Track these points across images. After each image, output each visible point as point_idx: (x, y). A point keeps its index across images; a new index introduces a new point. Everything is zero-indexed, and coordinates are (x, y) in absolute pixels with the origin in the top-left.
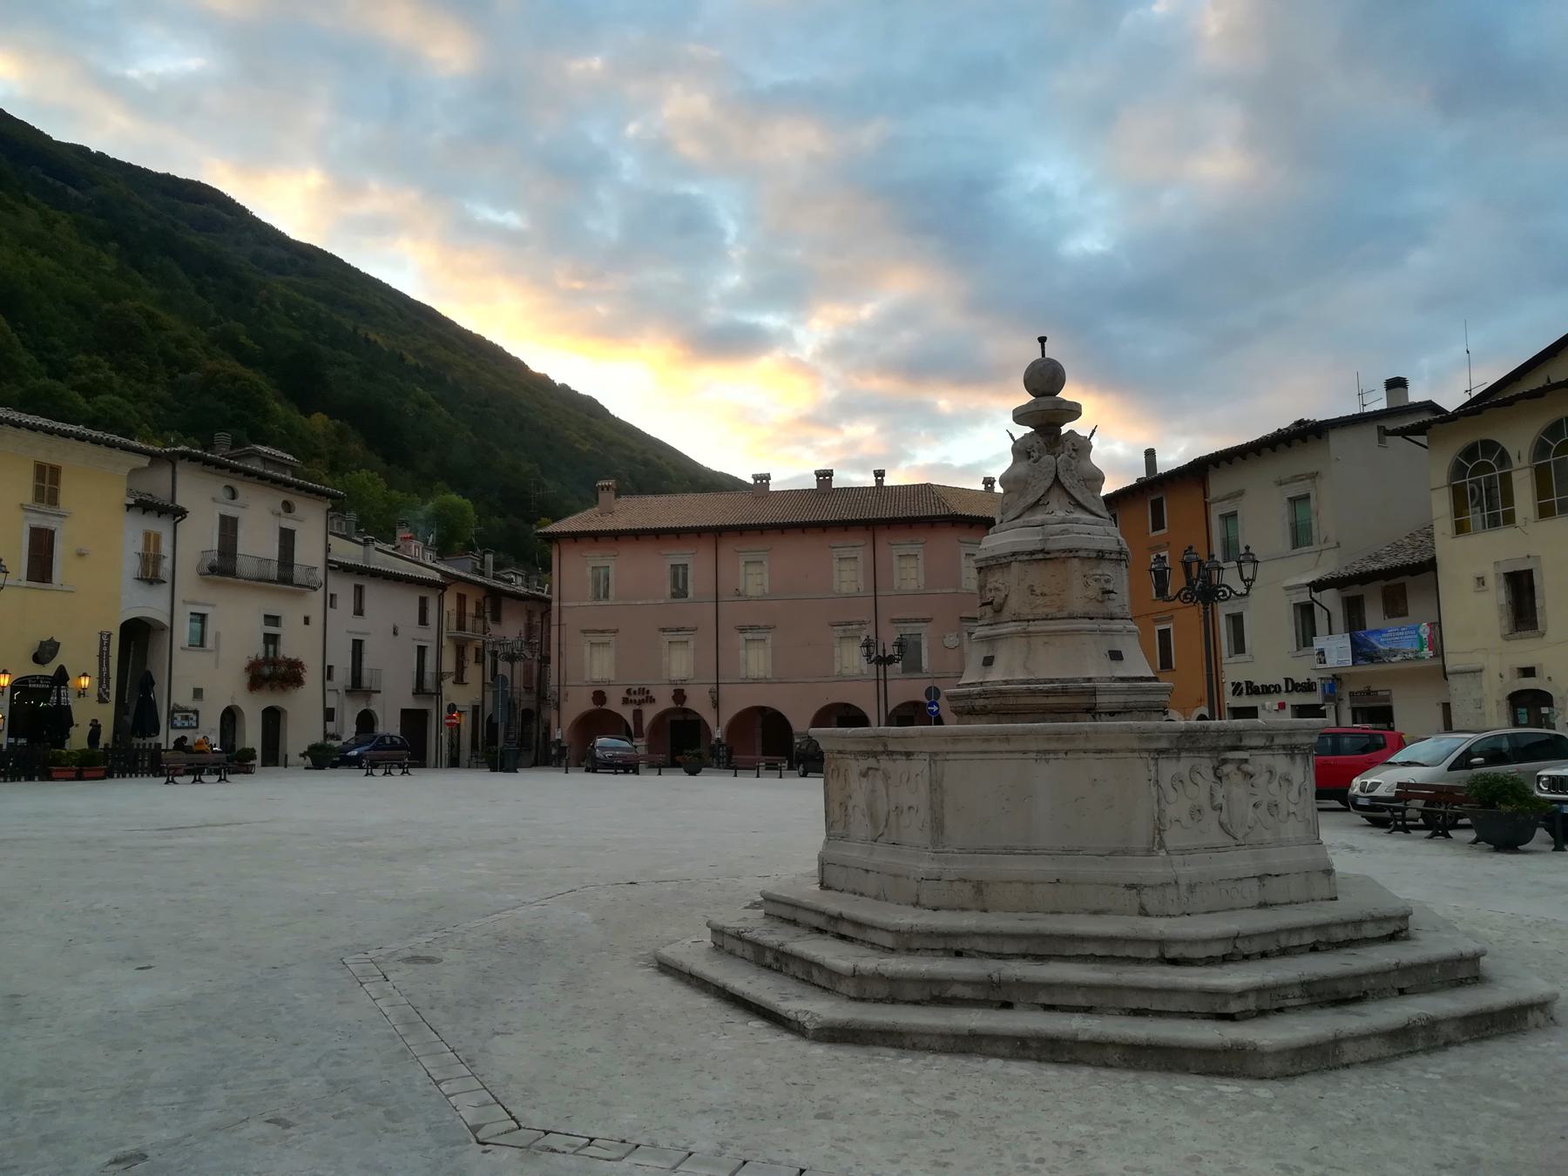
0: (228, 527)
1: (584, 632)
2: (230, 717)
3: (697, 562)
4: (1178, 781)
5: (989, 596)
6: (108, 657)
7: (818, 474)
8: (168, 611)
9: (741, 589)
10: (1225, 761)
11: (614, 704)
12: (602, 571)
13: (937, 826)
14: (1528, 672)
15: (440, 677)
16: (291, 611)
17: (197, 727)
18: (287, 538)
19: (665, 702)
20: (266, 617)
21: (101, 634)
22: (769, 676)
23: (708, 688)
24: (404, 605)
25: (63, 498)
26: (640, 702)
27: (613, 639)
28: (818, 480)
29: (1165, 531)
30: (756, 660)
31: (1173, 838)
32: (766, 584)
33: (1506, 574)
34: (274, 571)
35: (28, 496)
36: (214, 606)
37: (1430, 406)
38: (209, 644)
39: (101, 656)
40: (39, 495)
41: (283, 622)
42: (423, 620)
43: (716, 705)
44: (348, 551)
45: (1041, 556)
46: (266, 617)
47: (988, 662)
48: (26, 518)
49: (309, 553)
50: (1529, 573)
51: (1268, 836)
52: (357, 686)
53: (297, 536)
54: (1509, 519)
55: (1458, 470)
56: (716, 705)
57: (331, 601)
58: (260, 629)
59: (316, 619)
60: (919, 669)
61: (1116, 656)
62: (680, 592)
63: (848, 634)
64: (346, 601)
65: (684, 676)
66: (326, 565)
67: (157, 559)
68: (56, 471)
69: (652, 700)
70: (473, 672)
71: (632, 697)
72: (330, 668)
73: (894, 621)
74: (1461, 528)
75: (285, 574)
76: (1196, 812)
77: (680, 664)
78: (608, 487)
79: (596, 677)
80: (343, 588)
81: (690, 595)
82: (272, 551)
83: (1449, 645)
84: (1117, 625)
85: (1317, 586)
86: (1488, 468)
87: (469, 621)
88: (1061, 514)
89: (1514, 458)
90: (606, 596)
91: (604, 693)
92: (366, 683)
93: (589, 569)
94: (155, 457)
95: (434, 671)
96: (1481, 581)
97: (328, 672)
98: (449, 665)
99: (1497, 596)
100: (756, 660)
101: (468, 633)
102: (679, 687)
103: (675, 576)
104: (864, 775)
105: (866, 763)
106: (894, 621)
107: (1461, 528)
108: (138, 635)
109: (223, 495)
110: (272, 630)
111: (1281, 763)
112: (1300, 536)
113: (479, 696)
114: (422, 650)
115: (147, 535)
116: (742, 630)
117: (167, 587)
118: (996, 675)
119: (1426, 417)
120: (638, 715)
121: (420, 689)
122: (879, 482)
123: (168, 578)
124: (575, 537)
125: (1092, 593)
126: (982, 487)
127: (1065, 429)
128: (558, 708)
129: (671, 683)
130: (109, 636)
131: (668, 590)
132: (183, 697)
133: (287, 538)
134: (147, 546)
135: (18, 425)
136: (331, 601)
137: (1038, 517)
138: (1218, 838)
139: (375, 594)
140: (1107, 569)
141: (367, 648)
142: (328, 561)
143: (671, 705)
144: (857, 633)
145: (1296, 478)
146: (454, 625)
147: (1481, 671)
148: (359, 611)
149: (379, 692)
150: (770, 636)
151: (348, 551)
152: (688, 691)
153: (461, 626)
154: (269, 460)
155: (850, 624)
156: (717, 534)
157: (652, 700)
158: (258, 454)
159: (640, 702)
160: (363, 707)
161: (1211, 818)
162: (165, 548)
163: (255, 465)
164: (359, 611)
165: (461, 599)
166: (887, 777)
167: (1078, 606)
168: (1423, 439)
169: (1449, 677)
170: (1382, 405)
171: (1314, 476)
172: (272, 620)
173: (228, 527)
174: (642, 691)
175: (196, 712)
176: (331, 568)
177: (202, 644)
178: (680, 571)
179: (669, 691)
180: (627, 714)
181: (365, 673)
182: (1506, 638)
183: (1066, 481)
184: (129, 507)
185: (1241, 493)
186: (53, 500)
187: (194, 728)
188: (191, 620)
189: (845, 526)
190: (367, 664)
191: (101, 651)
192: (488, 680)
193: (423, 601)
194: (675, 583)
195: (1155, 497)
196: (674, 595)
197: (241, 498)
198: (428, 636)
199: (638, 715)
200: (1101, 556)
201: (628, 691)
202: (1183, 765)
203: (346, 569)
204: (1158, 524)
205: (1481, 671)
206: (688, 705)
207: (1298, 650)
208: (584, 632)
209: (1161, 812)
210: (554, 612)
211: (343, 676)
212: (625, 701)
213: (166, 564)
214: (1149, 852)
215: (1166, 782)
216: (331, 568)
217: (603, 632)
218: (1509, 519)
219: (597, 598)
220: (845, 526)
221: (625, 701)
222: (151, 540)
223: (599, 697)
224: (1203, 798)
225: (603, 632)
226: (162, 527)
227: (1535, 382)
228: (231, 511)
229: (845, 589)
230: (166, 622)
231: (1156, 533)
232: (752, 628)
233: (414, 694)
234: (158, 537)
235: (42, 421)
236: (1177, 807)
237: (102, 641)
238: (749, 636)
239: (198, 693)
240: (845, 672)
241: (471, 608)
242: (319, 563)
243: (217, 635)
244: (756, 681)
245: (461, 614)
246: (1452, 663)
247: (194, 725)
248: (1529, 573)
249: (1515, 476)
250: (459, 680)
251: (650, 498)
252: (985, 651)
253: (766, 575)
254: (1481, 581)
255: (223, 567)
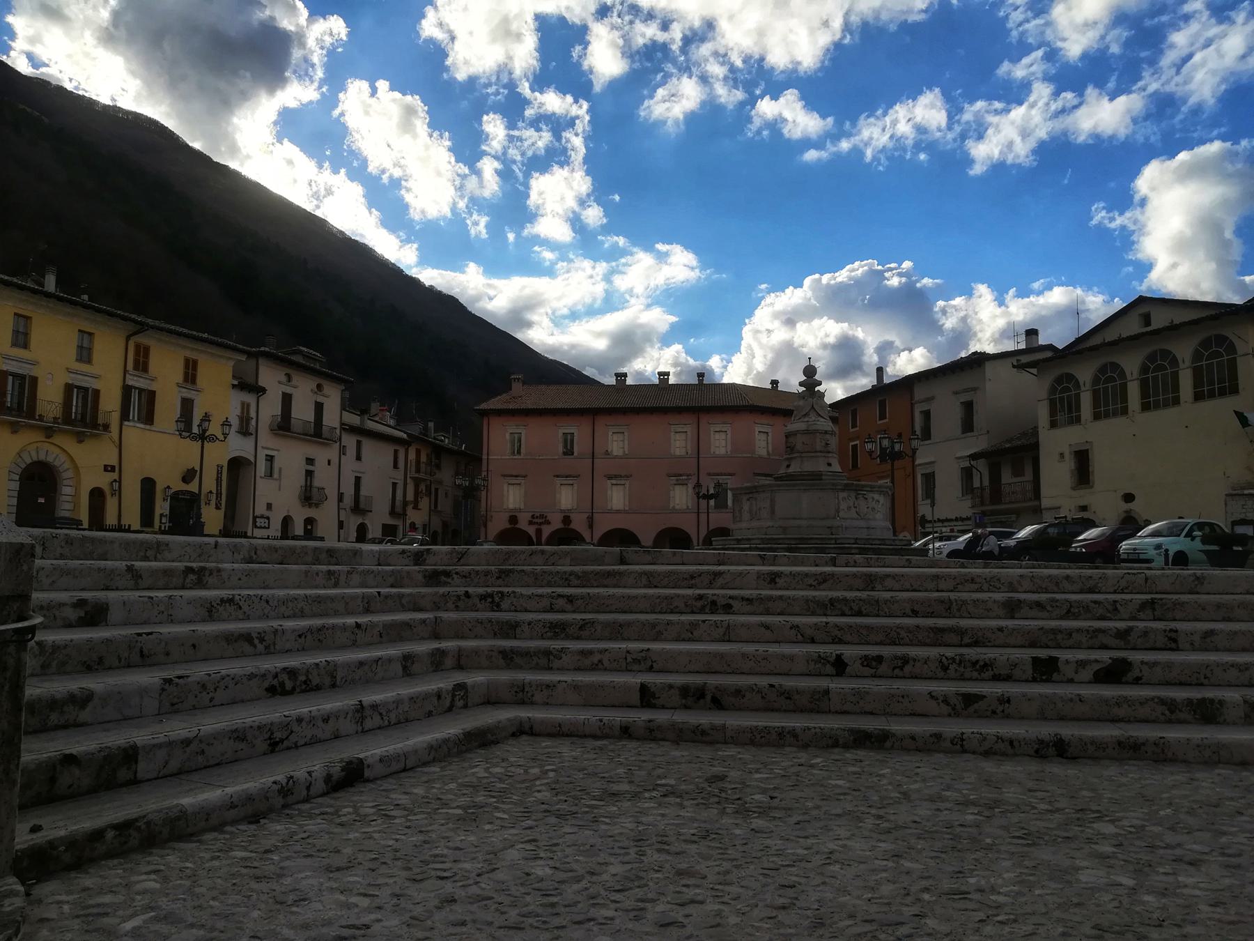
0: (287, 399)
1: (504, 476)
2: (287, 521)
3: (578, 430)
4: (844, 499)
5: (789, 445)
6: (221, 480)
7: (660, 374)
8: (253, 453)
9: (609, 450)
10: (859, 494)
11: (523, 525)
12: (516, 436)
13: (773, 512)
14: (1084, 508)
15: (405, 503)
16: (322, 455)
17: (269, 528)
18: (319, 408)
19: (557, 524)
20: (307, 459)
21: (218, 466)
22: (627, 508)
23: (586, 515)
24: (386, 452)
25: (198, 381)
26: (541, 524)
27: (523, 481)
28: (659, 378)
29: (887, 420)
30: (617, 498)
31: (841, 514)
32: (626, 446)
33: (1075, 452)
34: (312, 431)
35: (180, 378)
36: (278, 450)
37: (1050, 347)
38: (276, 475)
39: (217, 480)
40: (186, 380)
41: (317, 463)
42: (396, 466)
43: (591, 526)
44: (354, 419)
45: (807, 432)
46: (307, 459)
47: (788, 466)
48: (180, 392)
49: (332, 417)
50: (1087, 451)
51: (871, 517)
52: (357, 509)
53: (325, 407)
54: (1078, 420)
55: (1053, 390)
56: (591, 526)
57: (343, 450)
58: (303, 467)
59: (335, 461)
60: (726, 507)
61: (829, 465)
62: (569, 452)
63: (680, 482)
64: (351, 452)
65: (569, 507)
66: (341, 427)
67: (248, 419)
68: (195, 363)
69: (548, 523)
70: (424, 503)
71: (536, 520)
72: (342, 493)
73: (709, 474)
74: (1053, 425)
75: (317, 433)
76: (849, 508)
77: (566, 498)
78: (518, 379)
79: (511, 506)
80: (350, 441)
81: (575, 454)
82: (311, 417)
83: (1044, 491)
84: (830, 455)
85: (974, 457)
86: (1068, 389)
87: (423, 466)
88: (813, 418)
89: (1081, 384)
90: (519, 452)
91: (516, 517)
92: (362, 506)
93: (508, 436)
94: (250, 355)
95: (402, 499)
96: (1062, 455)
97: (341, 497)
98: (410, 497)
99: (1069, 464)
100: (617, 498)
101: (422, 476)
102: (568, 514)
103: (565, 441)
104: (748, 500)
105: (748, 496)
106: (709, 474)
107: (1053, 425)
108: (237, 465)
109: (284, 379)
110: (310, 468)
111: (876, 496)
112: (968, 426)
113: (427, 518)
114: (394, 484)
115: (243, 404)
116: (610, 478)
117: (254, 436)
118: (790, 470)
119: (1049, 354)
120: (539, 532)
121: (393, 513)
122: (701, 381)
123: (254, 432)
124: (500, 413)
125: (823, 444)
126: (769, 387)
127: (816, 389)
128: (486, 526)
129: (562, 511)
130: (222, 468)
131: (561, 449)
132: (261, 509)
133: (319, 408)
134: (243, 413)
135: (161, 329)
136: (343, 450)
137: (806, 419)
138: (855, 516)
139: (368, 445)
140: (828, 436)
141: (363, 482)
142: (342, 424)
143: (560, 526)
144: (686, 482)
145: (966, 391)
146: (413, 469)
147: (1059, 508)
148: (359, 458)
149: (371, 511)
150: (627, 483)
151: (354, 419)
152: (573, 516)
153: (418, 471)
154: (308, 357)
155: (681, 475)
156: (593, 413)
157: (548, 523)
158: (301, 352)
159: (541, 524)
160: (360, 521)
161: (853, 510)
162: (253, 414)
163: (298, 359)
164: (359, 458)
165: (418, 452)
166: (756, 499)
167: (818, 448)
168: (1034, 371)
169: (1044, 512)
170: (1022, 346)
171: (975, 389)
172: (310, 461)
173: (287, 399)
174: (542, 516)
175: (268, 518)
176: (344, 429)
177: (271, 476)
178: (569, 437)
179: (560, 517)
180: (531, 531)
181: (362, 499)
182: (1073, 489)
183: (815, 406)
184: (234, 386)
185: (932, 398)
186: (194, 381)
187: (265, 528)
188: (266, 460)
189: (679, 410)
190: (363, 492)
191: (218, 477)
192: (433, 508)
193: (396, 452)
194: (565, 446)
195: (881, 398)
196: (565, 454)
197: (294, 382)
198: (399, 476)
199: (539, 532)
200: (826, 432)
201: (533, 516)
202: (844, 494)
203: (353, 430)
204: (882, 417)
205: (1059, 508)
206: (573, 526)
207: (963, 496)
208: (504, 476)
209: (839, 507)
210: (484, 462)
211: (348, 500)
212: (531, 523)
213: (253, 422)
214: (834, 518)
215: (840, 498)
216: (344, 429)
217: (516, 476)
218: (1078, 420)
219: (513, 453)
220: (679, 410)
221: (531, 523)
222: (245, 407)
223: (513, 520)
224: (851, 504)
225: (516, 476)
226: (250, 398)
227: (1111, 335)
228: (288, 390)
229: (678, 452)
230: (252, 460)
231: (881, 422)
232: (616, 477)
233: (390, 514)
234: (248, 405)
235: (185, 331)
236: (843, 506)
237: (218, 471)
238: (614, 482)
239: (269, 506)
240: (677, 507)
241: (424, 458)
242: (337, 425)
243: (280, 470)
244: (618, 512)
245: (418, 462)
246: (1045, 503)
247: (267, 525)
248: (1087, 451)
249: (1082, 394)
250: (416, 507)
251: (543, 387)
252: (787, 463)
253: (626, 442)
254: (1062, 455)
255: (284, 426)
